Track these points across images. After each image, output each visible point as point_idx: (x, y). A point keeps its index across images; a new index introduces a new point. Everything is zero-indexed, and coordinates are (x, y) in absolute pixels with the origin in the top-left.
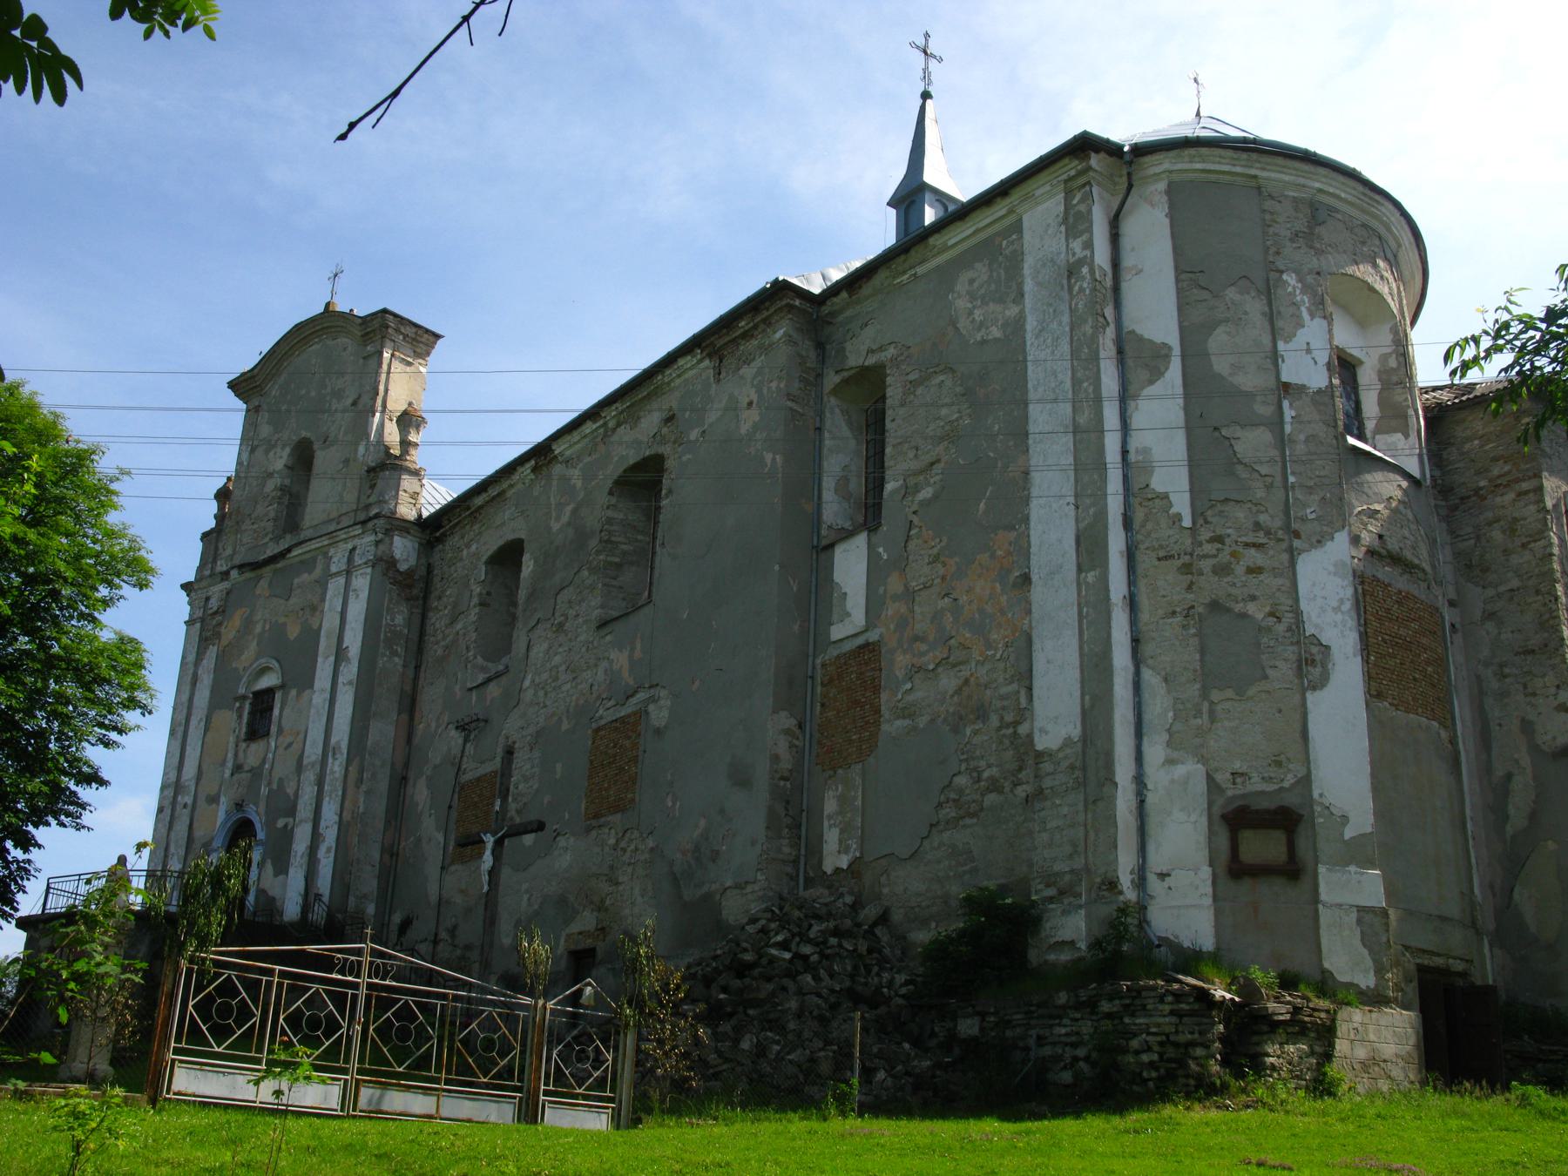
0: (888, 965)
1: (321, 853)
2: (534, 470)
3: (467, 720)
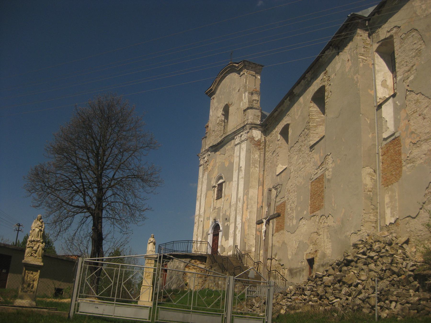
0: (408, 259)
1: (237, 232)
2: (290, 100)
3: (276, 185)
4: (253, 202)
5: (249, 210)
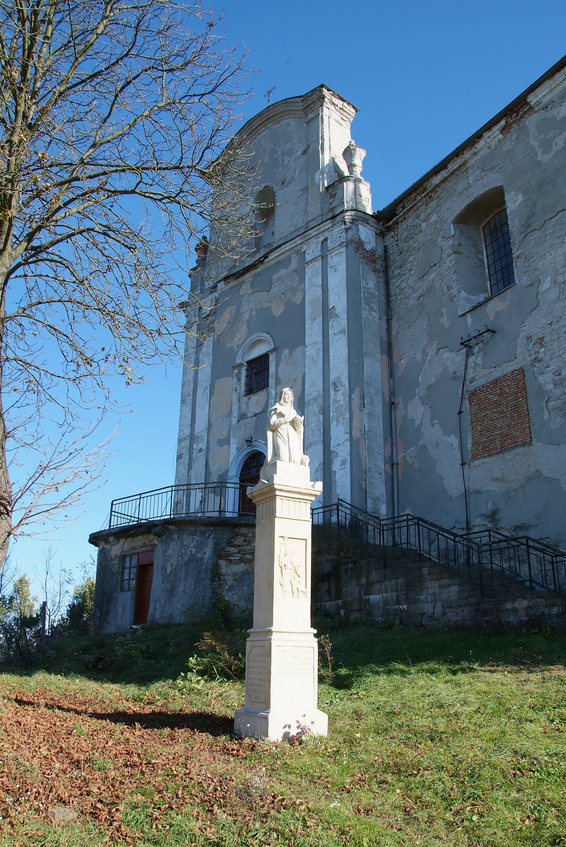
1: (336, 466)
2: (502, 131)
4: (373, 391)
5: (366, 409)
